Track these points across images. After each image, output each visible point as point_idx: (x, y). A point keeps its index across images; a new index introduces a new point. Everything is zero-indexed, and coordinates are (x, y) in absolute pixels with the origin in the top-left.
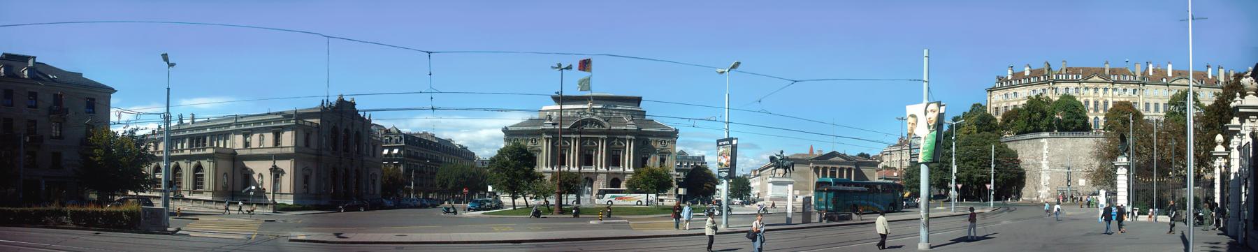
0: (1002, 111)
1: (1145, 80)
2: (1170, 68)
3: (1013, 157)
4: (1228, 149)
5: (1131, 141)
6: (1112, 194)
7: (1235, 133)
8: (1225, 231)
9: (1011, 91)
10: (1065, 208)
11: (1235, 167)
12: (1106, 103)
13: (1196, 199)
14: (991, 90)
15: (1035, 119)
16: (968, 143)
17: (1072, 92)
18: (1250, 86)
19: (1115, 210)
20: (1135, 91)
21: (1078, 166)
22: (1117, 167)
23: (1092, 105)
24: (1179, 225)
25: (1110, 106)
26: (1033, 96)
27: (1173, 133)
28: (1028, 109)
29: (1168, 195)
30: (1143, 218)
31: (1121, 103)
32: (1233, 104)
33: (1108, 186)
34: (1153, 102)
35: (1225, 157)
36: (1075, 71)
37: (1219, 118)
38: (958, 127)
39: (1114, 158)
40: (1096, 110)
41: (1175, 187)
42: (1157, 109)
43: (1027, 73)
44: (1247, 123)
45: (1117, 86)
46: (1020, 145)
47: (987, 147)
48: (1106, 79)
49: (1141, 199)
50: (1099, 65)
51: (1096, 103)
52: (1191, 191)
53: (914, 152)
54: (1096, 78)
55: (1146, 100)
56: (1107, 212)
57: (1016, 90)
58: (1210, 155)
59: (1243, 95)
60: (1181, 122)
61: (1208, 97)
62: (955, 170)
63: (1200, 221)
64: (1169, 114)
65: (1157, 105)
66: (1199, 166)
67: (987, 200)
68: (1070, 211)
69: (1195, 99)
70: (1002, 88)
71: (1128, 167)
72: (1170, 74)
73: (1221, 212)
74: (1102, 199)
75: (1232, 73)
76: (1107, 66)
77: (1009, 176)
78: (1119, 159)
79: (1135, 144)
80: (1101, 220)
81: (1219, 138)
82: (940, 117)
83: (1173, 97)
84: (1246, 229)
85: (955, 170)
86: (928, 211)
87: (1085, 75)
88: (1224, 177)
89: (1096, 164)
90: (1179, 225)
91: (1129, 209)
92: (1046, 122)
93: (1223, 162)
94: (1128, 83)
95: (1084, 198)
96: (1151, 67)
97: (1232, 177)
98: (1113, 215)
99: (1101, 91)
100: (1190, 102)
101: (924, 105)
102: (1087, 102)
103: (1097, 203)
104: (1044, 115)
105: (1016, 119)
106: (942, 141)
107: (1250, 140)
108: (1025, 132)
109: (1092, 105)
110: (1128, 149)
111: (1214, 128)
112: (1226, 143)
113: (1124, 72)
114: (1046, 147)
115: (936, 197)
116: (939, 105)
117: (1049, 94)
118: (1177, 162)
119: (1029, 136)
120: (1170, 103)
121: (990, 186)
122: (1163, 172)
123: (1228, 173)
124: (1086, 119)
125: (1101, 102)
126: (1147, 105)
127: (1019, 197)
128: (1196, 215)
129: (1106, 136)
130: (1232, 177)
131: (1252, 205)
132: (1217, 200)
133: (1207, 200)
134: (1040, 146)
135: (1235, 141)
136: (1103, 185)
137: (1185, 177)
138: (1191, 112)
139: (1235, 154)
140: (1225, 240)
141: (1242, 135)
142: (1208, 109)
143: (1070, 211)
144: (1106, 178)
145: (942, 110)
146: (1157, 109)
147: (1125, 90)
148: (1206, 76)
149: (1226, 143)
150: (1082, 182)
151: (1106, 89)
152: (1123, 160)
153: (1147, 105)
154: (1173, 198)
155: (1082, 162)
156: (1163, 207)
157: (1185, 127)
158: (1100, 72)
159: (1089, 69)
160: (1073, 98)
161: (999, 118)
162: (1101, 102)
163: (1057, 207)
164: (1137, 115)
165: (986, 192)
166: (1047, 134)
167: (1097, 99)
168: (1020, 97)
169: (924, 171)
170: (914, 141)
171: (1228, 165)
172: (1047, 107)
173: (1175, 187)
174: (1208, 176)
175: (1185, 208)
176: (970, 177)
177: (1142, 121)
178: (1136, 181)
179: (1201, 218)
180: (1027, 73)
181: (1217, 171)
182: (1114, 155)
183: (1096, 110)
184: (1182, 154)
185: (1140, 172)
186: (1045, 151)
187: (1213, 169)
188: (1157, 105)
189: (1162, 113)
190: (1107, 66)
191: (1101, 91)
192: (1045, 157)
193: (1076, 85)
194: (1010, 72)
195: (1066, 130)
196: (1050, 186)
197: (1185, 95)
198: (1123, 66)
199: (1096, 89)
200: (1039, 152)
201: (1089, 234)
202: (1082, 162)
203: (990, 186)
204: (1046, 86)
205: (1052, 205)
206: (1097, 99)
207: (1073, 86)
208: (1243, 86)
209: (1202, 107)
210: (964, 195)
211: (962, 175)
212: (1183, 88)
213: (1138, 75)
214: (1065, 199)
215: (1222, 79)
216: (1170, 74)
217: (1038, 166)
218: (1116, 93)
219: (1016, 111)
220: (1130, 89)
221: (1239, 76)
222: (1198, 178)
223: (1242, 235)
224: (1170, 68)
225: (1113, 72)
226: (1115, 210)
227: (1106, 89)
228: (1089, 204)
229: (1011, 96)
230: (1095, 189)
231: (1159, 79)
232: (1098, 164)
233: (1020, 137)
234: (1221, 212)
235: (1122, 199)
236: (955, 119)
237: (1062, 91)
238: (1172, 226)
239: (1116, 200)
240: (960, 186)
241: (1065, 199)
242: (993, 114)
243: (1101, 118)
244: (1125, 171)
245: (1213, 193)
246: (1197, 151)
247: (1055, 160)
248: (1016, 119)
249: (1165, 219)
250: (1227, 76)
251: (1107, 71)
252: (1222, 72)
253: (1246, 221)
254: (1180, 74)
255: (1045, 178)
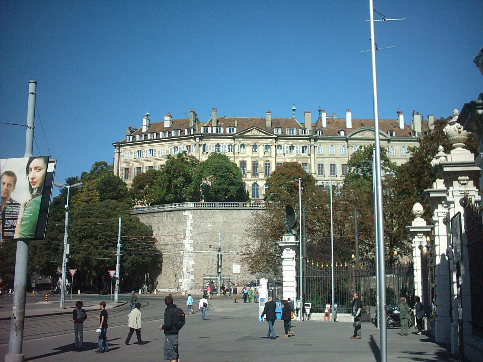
0: (133, 174)
1: (316, 135)
2: (349, 116)
3: (147, 234)
4: (431, 223)
5: (300, 214)
6: (276, 285)
7: (439, 200)
8: (430, 336)
9: (146, 148)
10: (213, 302)
11: (442, 247)
12: (267, 165)
13: (389, 292)
14: (120, 145)
15: (177, 185)
16: (86, 214)
17: (224, 150)
18: (456, 136)
19: (279, 306)
20: (304, 148)
21: (231, 247)
22: (282, 248)
23: (249, 167)
24: (366, 327)
25: (273, 168)
26: (175, 154)
27: (355, 202)
28: (168, 171)
29: (351, 286)
30: (317, 317)
31: (286, 165)
32: (434, 162)
33: (271, 274)
34: (327, 162)
35: (426, 234)
36: (229, 123)
37: (416, 181)
38: (74, 191)
39: (278, 236)
40: (255, 174)
41: (360, 275)
42: (333, 171)
43: (167, 124)
44: (456, 187)
45: (281, 142)
46: (156, 217)
47: (112, 220)
48: (268, 134)
49: (315, 291)
50: (258, 116)
51: (255, 165)
52: (381, 281)
53: (7, 224)
54: (255, 132)
55: (319, 161)
56: (270, 309)
57: (153, 146)
58: (406, 231)
59: (448, 149)
60: (365, 188)
61: (400, 154)
62: (67, 249)
63: (395, 321)
64: (349, 178)
65: (333, 166)
66: (391, 247)
67: (109, 291)
68: (221, 307)
69: (383, 157)
70: (134, 143)
71: (296, 248)
72: (349, 125)
73: (425, 309)
74: (263, 291)
75: (431, 120)
76: (269, 117)
77: (140, 259)
78: (285, 237)
79: (306, 219)
80: (262, 319)
81: (418, 208)
82: (48, 178)
83: (355, 156)
84: (461, 334)
85: (67, 249)
86: (23, 306)
87: (243, 129)
88: (427, 260)
89: (255, 245)
90: (366, 327)
91: (298, 305)
92: (190, 189)
93: (425, 240)
94: (296, 138)
95: (239, 290)
96: (324, 116)
97: (438, 261)
98: (278, 313)
99: (261, 149)
100: (377, 162)
101: (26, 160)
102: (243, 164)
103: (256, 297)
104: (188, 179)
105: (152, 184)
106: (49, 211)
107: (461, 210)
108: (163, 202)
109: (249, 167)
110: (295, 226)
111: (410, 194)
112: (428, 215)
113: (291, 124)
114: (189, 222)
115: (41, 287)
116: (47, 161)
117: (195, 152)
118: (361, 242)
119: (168, 207)
120: (351, 164)
121: (115, 273)
122: (343, 255)
123: (432, 255)
124: (242, 185)
125: (261, 163)
126: (321, 167)
127: (151, 290)
128: (389, 313)
129: (268, 208)
130: (438, 261)
131: (468, 300)
132: (419, 292)
133: (403, 292)
134: (182, 221)
135: (440, 212)
136: (263, 272)
137: (373, 261)
138: (379, 175)
139: (441, 230)
140: (431, 350)
141: (449, 204)
142: (401, 170)
143: (221, 307)
144: (267, 262)
145: (51, 168)
146: (333, 171)
147: (292, 147)
148: (397, 125)
149: (428, 215)
150: (236, 268)
151: (267, 147)
152: (290, 239)
153: (321, 167)
154: (358, 289)
155: (237, 242)
156: (344, 302)
157: (371, 195)
158: (260, 125)
159: (246, 121)
160: (225, 158)
161: (129, 182)
162: (261, 163)
163: (203, 301)
164: (308, 180)
165: (110, 280)
166: (191, 205)
167: (256, 159)
168: (158, 155)
169: (21, 252)
170: (9, 208)
171: (432, 245)
172: (191, 170)
173: (360, 275)
174: (404, 260)
175: (374, 304)
176: (87, 261)
177: (314, 189)
178: (307, 267)
179: (396, 318)
180: (167, 124)
181: (417, 253)
182: (278, 232)
183: (255, 174)
184: (367, 231)
185: (313, 254)
186: (189, 228)
187: (411, 250)
188: (333, 166)
189: (340, 177)
190: (269, 117)
191: (261, 149)
192: (188, 234)
193: (229, 141)
194: (145, 122)
195: (217, 200)
196: (194, 273)
197: (370, 152)
198: (288, 116)
199: (255, 146)
200: (180, 228)
201: (245, 339)
202: (237, 242)
203: (115, 273)
204: (191, 142)
205: (196, 299)
206: (256, 159)
207: (225, 142)
208: (447, 137)
209: (393, 167)
210: (79, 284)
211: (77, 257)
212: (367, 144)
213: (309, 127)
214: (214, 290)
215: (418, 128)
216: (349, 125)
217: (179, 246)
218: (280, 152)
219: (152, 174)
220: (298, 145)
221: (441, 123)
222: (390, 262)
223: (455, 343)
224: (349, 116)
225: (276, 123)
226: (279, 306)
227: (267, 147)
228: (245, 297)
229: (146, 154)
230: (254, 278)
231: (336, 131)
232: (257, 244)
233: (157, 208)
234: (425, 309)
235: (289, 291)
236: (71, 181)
237: (211, 149)
238: (357, 328)
239: (281, 292)
240: (73, 272)
241: (214, 290)
242: (122, 176)
243: (262, 184)
244: (292, 253)
245: (412, 283)
246: (387, 226)
247: (201, 238)
248: (152, 184)
249: (347, 318)
250: (424, 123)
251: (269, 123)
252: (417, 119)
253: (461, 322)
254: (363, 125)
255: (188, 263)
